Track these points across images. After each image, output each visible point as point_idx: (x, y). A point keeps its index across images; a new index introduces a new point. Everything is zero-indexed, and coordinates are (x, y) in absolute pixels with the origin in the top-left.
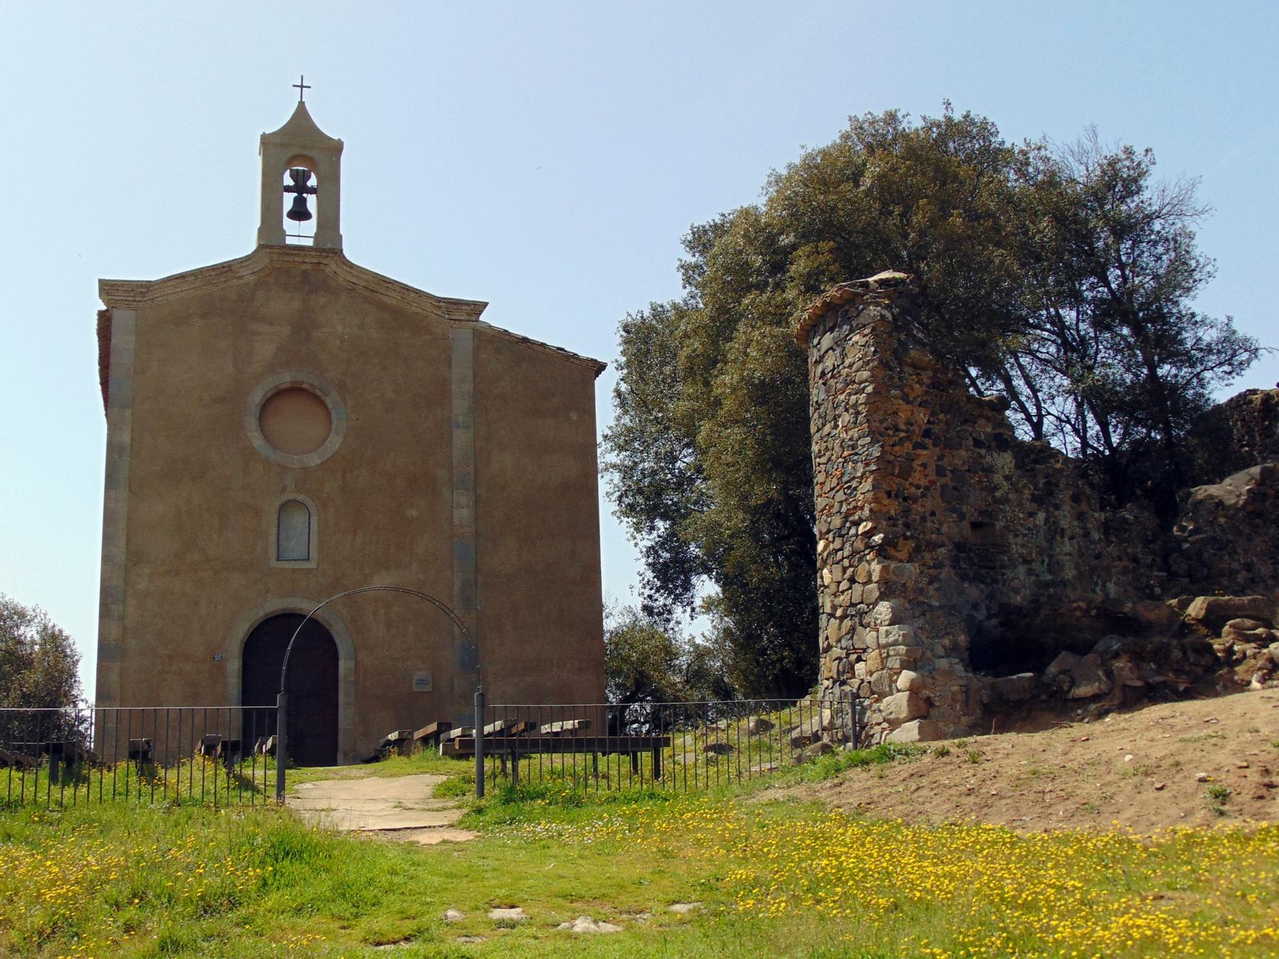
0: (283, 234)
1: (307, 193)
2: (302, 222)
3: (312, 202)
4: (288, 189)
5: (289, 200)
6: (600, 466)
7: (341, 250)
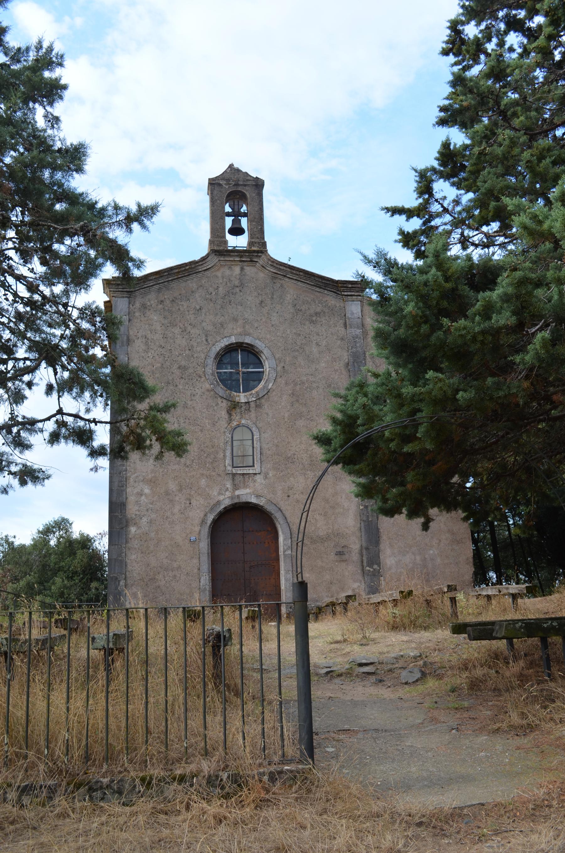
0: (226, 242)
1: (241, 217)
2: (238, 237)
3: (244, 222)
4: (228, 214)
5: (229, 222)
6: (295, 667)
7: (266, 251)
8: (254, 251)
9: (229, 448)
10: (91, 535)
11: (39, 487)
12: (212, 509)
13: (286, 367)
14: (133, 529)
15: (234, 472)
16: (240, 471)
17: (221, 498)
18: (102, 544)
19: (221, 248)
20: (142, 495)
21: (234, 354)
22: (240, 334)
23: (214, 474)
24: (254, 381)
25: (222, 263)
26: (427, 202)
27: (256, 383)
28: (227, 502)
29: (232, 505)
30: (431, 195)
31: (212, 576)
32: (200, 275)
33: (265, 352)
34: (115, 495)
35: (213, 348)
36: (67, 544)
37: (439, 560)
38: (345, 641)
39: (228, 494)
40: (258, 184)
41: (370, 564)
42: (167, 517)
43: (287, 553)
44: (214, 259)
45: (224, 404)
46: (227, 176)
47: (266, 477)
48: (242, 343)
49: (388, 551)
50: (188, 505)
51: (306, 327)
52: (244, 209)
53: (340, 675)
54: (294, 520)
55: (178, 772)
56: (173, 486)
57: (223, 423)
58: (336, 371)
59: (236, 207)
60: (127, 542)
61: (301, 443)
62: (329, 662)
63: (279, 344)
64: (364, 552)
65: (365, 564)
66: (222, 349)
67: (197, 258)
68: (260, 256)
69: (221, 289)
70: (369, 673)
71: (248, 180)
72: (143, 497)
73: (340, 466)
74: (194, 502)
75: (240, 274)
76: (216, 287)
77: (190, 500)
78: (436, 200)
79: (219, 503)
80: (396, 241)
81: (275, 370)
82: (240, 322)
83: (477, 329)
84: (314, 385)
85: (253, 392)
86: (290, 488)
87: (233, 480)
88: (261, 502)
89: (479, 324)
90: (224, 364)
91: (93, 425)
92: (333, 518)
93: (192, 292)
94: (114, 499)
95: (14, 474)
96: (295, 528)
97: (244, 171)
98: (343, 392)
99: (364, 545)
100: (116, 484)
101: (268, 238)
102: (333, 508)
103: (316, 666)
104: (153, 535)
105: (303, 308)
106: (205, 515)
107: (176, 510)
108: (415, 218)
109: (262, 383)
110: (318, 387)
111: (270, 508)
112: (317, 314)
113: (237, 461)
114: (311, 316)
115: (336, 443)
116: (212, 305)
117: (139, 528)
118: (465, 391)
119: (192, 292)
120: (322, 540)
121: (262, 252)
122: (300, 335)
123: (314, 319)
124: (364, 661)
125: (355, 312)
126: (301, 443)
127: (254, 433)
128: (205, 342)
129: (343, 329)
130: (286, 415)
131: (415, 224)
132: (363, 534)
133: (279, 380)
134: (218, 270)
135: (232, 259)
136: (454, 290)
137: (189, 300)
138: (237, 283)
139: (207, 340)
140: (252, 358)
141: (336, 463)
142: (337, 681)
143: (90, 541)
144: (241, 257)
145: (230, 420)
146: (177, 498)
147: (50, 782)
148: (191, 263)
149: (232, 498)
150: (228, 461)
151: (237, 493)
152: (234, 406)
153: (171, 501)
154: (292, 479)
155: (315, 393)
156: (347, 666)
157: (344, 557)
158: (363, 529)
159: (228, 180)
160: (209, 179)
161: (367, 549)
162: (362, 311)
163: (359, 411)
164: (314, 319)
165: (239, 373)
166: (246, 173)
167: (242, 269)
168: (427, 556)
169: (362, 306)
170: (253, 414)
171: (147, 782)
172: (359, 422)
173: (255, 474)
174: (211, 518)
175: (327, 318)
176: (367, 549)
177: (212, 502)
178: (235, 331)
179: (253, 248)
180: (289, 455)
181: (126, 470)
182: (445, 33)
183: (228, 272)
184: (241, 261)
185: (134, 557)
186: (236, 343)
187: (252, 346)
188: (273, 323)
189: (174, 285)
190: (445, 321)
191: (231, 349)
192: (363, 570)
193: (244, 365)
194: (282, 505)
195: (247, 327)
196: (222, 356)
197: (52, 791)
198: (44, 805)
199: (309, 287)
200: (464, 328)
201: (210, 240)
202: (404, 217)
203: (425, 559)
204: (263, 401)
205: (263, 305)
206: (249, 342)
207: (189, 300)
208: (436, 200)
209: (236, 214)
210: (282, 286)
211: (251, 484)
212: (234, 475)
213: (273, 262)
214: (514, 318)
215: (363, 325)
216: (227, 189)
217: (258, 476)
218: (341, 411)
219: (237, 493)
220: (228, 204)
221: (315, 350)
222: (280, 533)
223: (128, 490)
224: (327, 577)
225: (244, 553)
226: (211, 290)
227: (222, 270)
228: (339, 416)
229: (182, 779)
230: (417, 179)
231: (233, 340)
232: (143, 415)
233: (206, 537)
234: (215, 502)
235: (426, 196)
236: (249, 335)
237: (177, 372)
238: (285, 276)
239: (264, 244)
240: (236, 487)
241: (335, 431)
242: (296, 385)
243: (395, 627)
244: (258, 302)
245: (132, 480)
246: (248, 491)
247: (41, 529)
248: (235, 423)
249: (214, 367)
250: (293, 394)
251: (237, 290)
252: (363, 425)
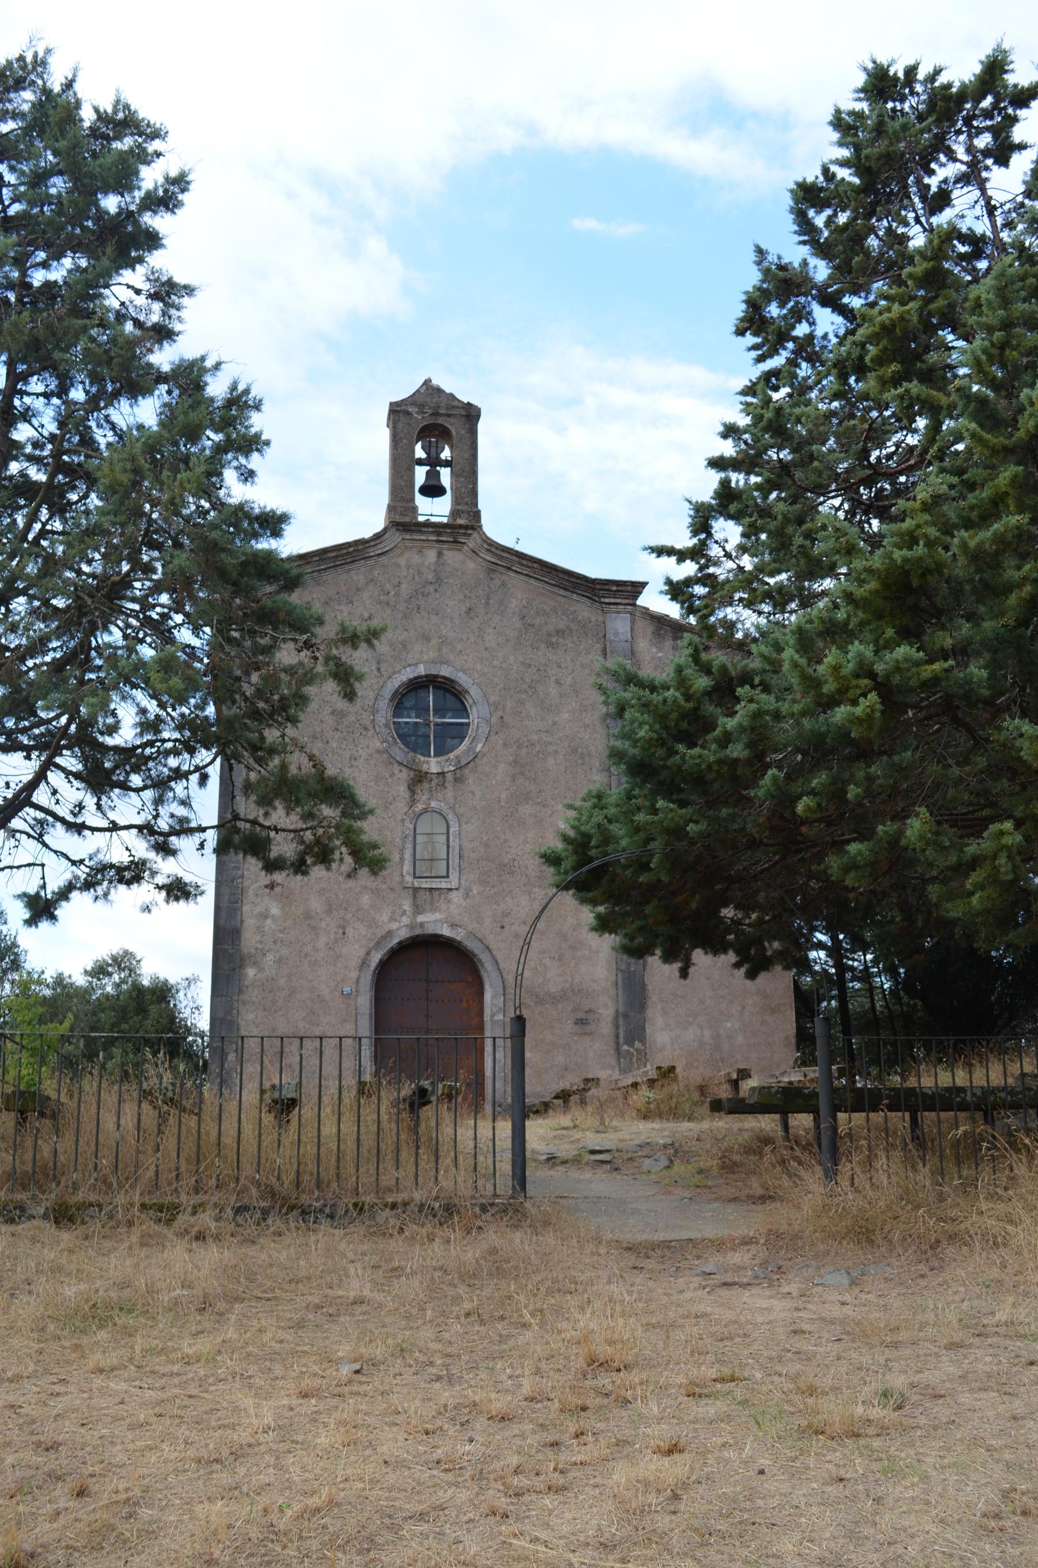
0: (414, 509)
3: (445, 476)
4: (420, 462)
5: (420, 474)
8: (461, 526)
9: (409, 846)
10: (172, 981)
11: (191, 904)
12: (378, 944)
13: (505, 719)
14: (251, 972)
15: (416, 885)
16: (425, 884)
17: (394, 926)
18: (189, 995)
19: (407, 519)
20: (266, 917)
21: (422, 693)
22: (434, 662)
23: (384, 887)
24: (454, 738)
25: (407, 543)
26: (703, 544)
27: (456, 741)
28: (403, 934)
29: (412, 938)
30: (710, 535)
31: (376, 1051)
32: (371, 562)
33: (472, 692)
34: (223, 915)
35: (389, 683)
36: (134, 994)
37: (740, 1039)
38: (575, 1127)
39: (405, 920)
40: (471, 415)
41: (630, 1042)
42: (307, 955)
43: (496, 1018)
44: (395, 538)
45: (404, 775)
46: (420, 399)
47: (467, 895)
48: (437, 676)
49: (660, 1022)
50: (340, 935)
51: (540, 653)
52: (446, 454)
53: (565, 1162)
54: (509, 966)
55: (390, 1200)
56: (316, 905)
57: (401, 806)
58: (587, 726)
59: (433, 451)
60: (240, 992)
61: (526, 842)
62: (552, 1149)
63: (496, 680)
64: (621, 1022)
65: (621, 1040)
66: (403, 684)
67: (367, 534)
68: (470, 535)
69: (404, 586)
70: (602, 1162)
71: (454, 407)
72: (269, 921)
73: (571, 892)
74: (350, 932)
75: (436, 563)
76: (396, 582)
77: (344, 928)
78: (716, 542)
79: (390, 934)
80: (661, 592)
81: (488, 722)
82: (434, 642)
83: (712, 759)
84: (551, 749)
85: (452, 756)
86: (506, 914)
87: (415, 897)
88: (459, 935)
89: (715, 752)
90: (405, 708)
91: (272, 834)
92: (573, 963)
93: (358, 590)
94: (222, 922)
95: (159, 888)
96: (510, 979)
97: (448, 391)
98: (578, 803)
99: (621, 1009)
100: (226, 897)
101: (484, 504)
102: (573, 948)
103: (533, 1151)
104: (282, 982)
105: (538, 621)
106: (368, 953)
107: (321, 943)
108: (688, 561)
109: (466, 742)
110: (556, 752)
111: (472, 945)
112: (559, 632)
113: (422, 868)
114: (549, 635)
115: (566, 865)
116: (389, 611)
117: (261, 970)
118: (697, 822)
119: (358, 590)
120: (555, 999)
121: (473, 528)
122: (530, 666)
123: (554, 640)
124: (598, 1148)
125: (621, 631)
126: (526, 842)
127: (451, 823)
128: (376, 673)
129: (601, 659)
130: (503, 796)
131: (689, 568)
132: (620, 992)
133: (493, 738)
134: (401, 555)
135: (423, 537)
136: (696, 709)
137: (351, 602)
138: (430, 577)
139: (379, 670)
140: (451, 701)
141: (566, 888)
142: (561, 1168)
143: (170, 990)
144: (439, 534)
145: (413, 801)
146: (323, 925)
147: (263, 1204)
148: (357, 543)
149: (411, 927)
150: (407, 867)
151: (420, 919)
152: (419, 778)
153: (314, 928)
154: (508, 899)
155: (551, 762)
156: (576, 1153)
157: (588, 1028)
158: (620, 984)
159: (421, 407)
160: (391, 404)
161: (626, 1016)
162: (632, 630)
163: (593, 831)
164: (554, 640)
165: (428, 725)
166: (452, 395)
167: (440, 554)
168: (721, 1031)
169: (633, 622)
170: (449, 793)
171: (360, 1208)
172: (593, 843)
173: (450, 890)
174: (376, 958)
175: (575, 639)
176: (626, 1016)
177: (380, 932)
178: (426, 657)
179: (460, 521)
180: (506, 861)
181: (242, 876)
182: (738, 309)
183: (416, 559)
184: (438, 541)
185: (251, 1016)
186: (427, 676)
187: (452, 681)
188: (488, 645)
189: (329, 576)
190: (681, 747)
191: (418, 685)
192: (618, 1049)
193: (439, 711)
194: (492, 941)
195: (445, 650)
196: (403, 695)
197: (265, 1213)
198: (258, 1224)
199: (547, 587)
200: (700, 756)
201: (389, 506)
202: (674, 559)
203: (719, 1035)
204: (466, 771)
205: (472, 614)
206: (447, 675)
207: (351, 602)
208: (716, 542)
209: (433, 462)
210: (503, 584)
211: (444, 906)
212: (416, 890)
213: (490, 545)
214: (747, 751)
215: (633, 653)
216: (420, 419)
217: (455, 892)
218: (573, 827)
219: (420, 919)
220: (419, 444)
221: (553, 690)
222: (487, 986)
223: (246, 908)
224: (560, 1059)
225: (427, 1016)
226: (388, 587)
227: (407, 555)
228: (572, 833)
229: (394, 1206)
230: (692, 513)
231: (422, 670)
232: (334, 822)
233: (368, 988)
234: (384, 932)
235: (703, 536)
236: (447, 662)
237: (330, 721)
238: (509, 568)
239: (477, 515)
240: (418, 909)
241: (566, 850)
242: (520, 747)
243: (646, 1115)
244: (464, 609)
245: (251, 892)
246: (437, 916)
247: (89, 968)
248: (420, 807)
249: (390, 714)
250: (515, 761)
251: (431, 588)
252: (597, 847)
